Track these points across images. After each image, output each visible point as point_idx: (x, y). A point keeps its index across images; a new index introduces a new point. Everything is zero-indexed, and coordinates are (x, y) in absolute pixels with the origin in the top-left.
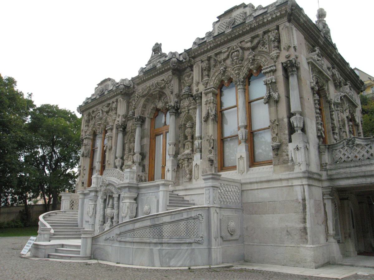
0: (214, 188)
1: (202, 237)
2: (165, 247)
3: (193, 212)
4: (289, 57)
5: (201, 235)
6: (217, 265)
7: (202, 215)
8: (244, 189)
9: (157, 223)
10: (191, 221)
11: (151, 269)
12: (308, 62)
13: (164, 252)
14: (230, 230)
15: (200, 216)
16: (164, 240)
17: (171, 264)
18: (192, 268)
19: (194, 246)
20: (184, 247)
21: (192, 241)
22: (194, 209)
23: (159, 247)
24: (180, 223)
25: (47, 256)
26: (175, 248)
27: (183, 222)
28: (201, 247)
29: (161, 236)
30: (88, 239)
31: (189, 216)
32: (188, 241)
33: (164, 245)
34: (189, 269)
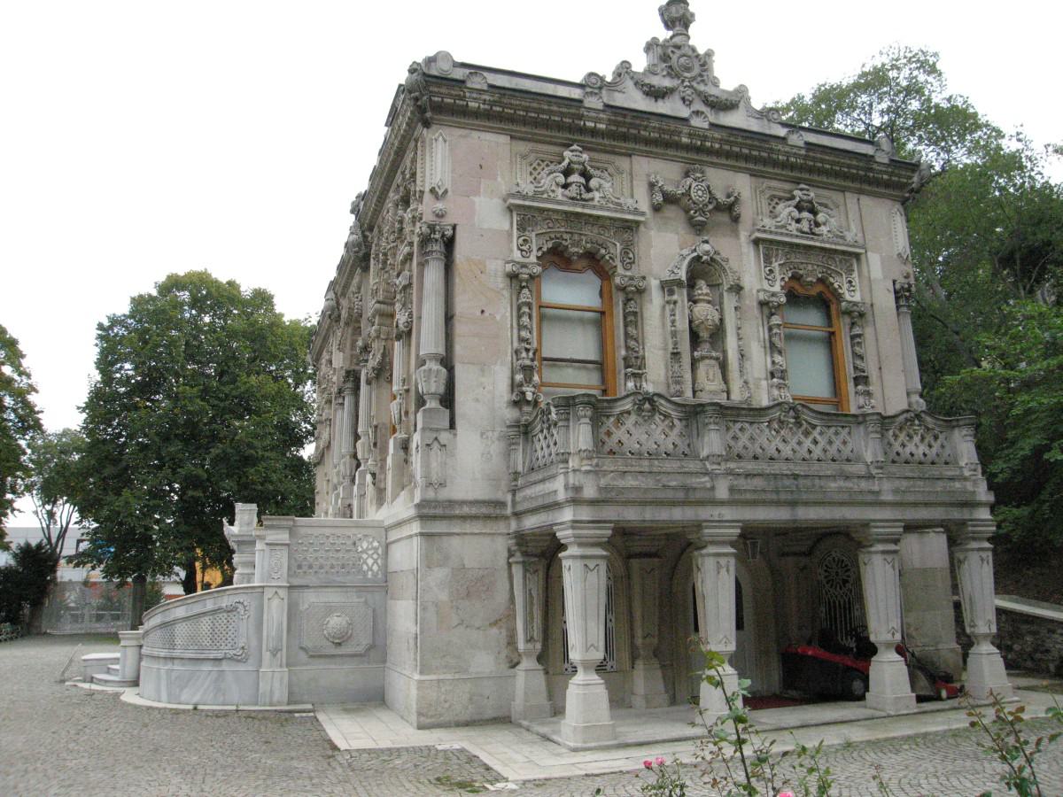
0: (272, 547)
1: (243, 648)
2: (177, 667)
3: (226, 598)
4: (442, 216)
5: (241, 645)
6: (271, 705)
7: (245, 603)
8: (391, 539)
9: (167, 620)
10: (221, 616)
11: (165, 709)
12: (508, 208)
13: (174, 675)
14: (329, 634)
15: (240, 606)
16: (177, 653)
17: (184, 697)
18: (200, 707)
19: (225, 666)
20: (207, 667)
21: (220, 656)
22: (228, 593)
23: (169, 666)
24: (202, 619)
25: (89, 679)
26: (190, 667)
27: (207, 618)
28: (241, 667)
29: (172, 646)
30: (128, 649)
31: (216, 607)
32: (212, 656)
33: (176, 662)
34: (195, 709)
